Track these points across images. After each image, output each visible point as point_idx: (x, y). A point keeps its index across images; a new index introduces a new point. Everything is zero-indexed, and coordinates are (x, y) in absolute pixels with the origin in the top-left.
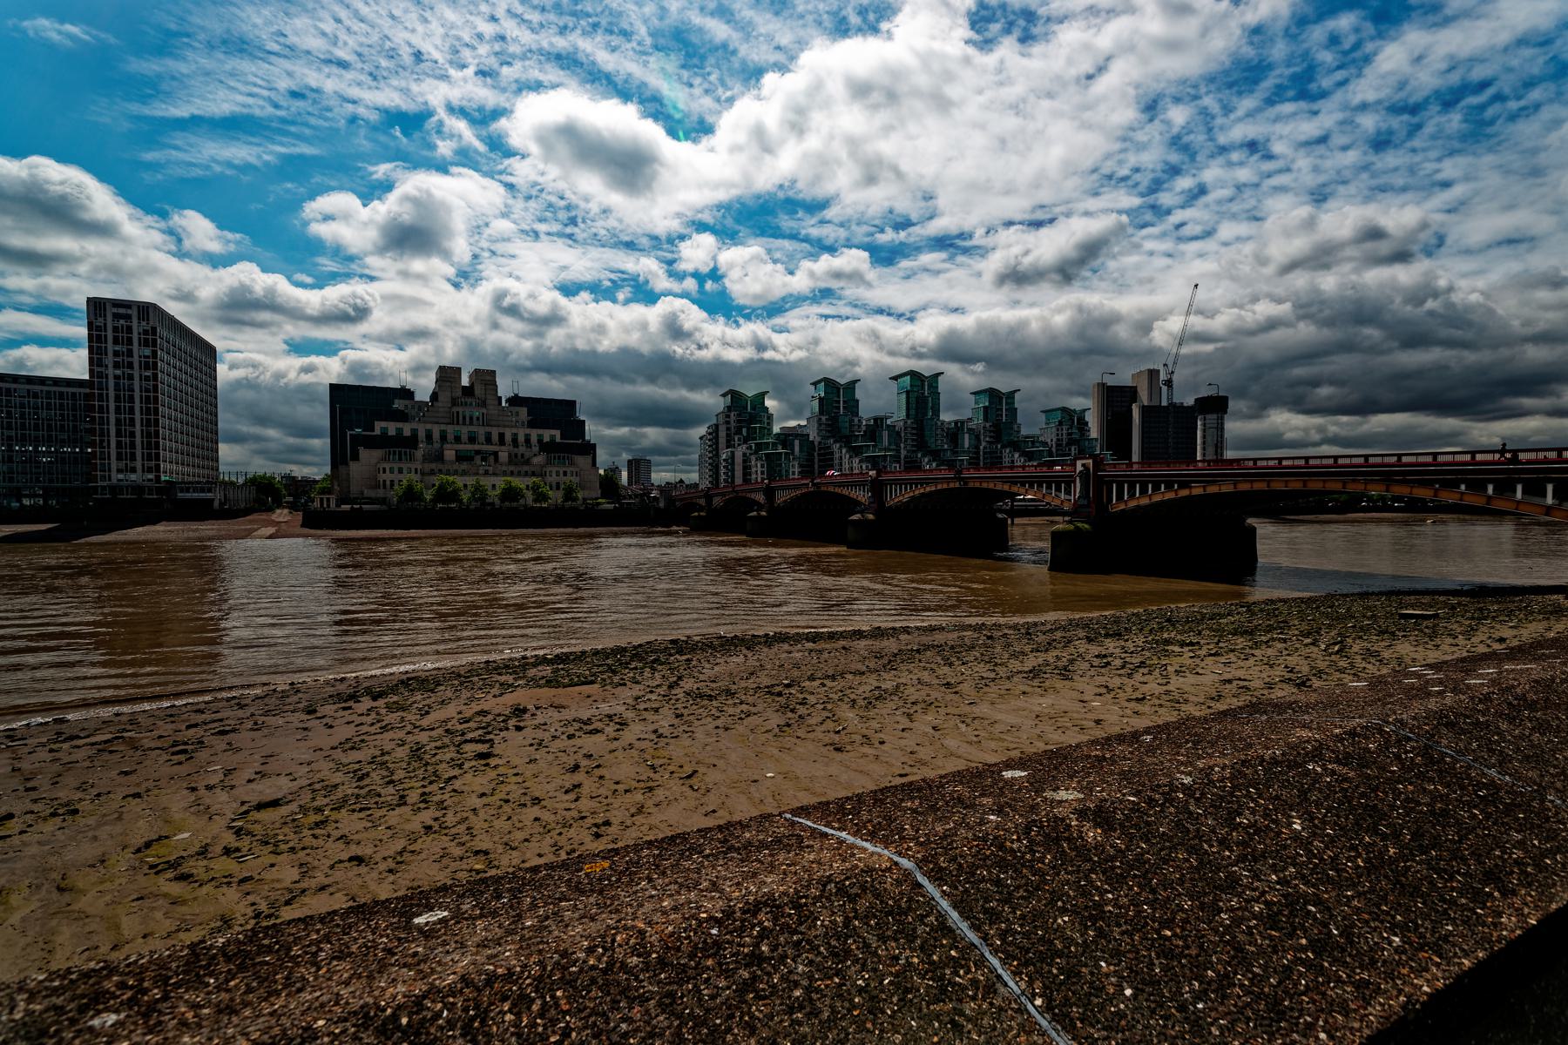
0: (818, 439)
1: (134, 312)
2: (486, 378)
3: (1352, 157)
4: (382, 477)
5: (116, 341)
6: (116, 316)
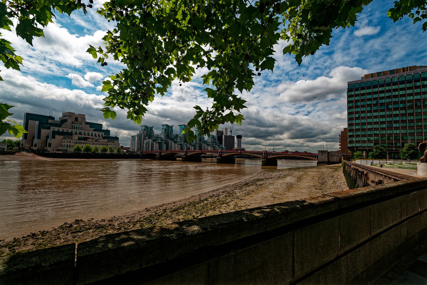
0: (164, 139)
2: (83, 117)
3: (260, 87)
4: (63, 144)
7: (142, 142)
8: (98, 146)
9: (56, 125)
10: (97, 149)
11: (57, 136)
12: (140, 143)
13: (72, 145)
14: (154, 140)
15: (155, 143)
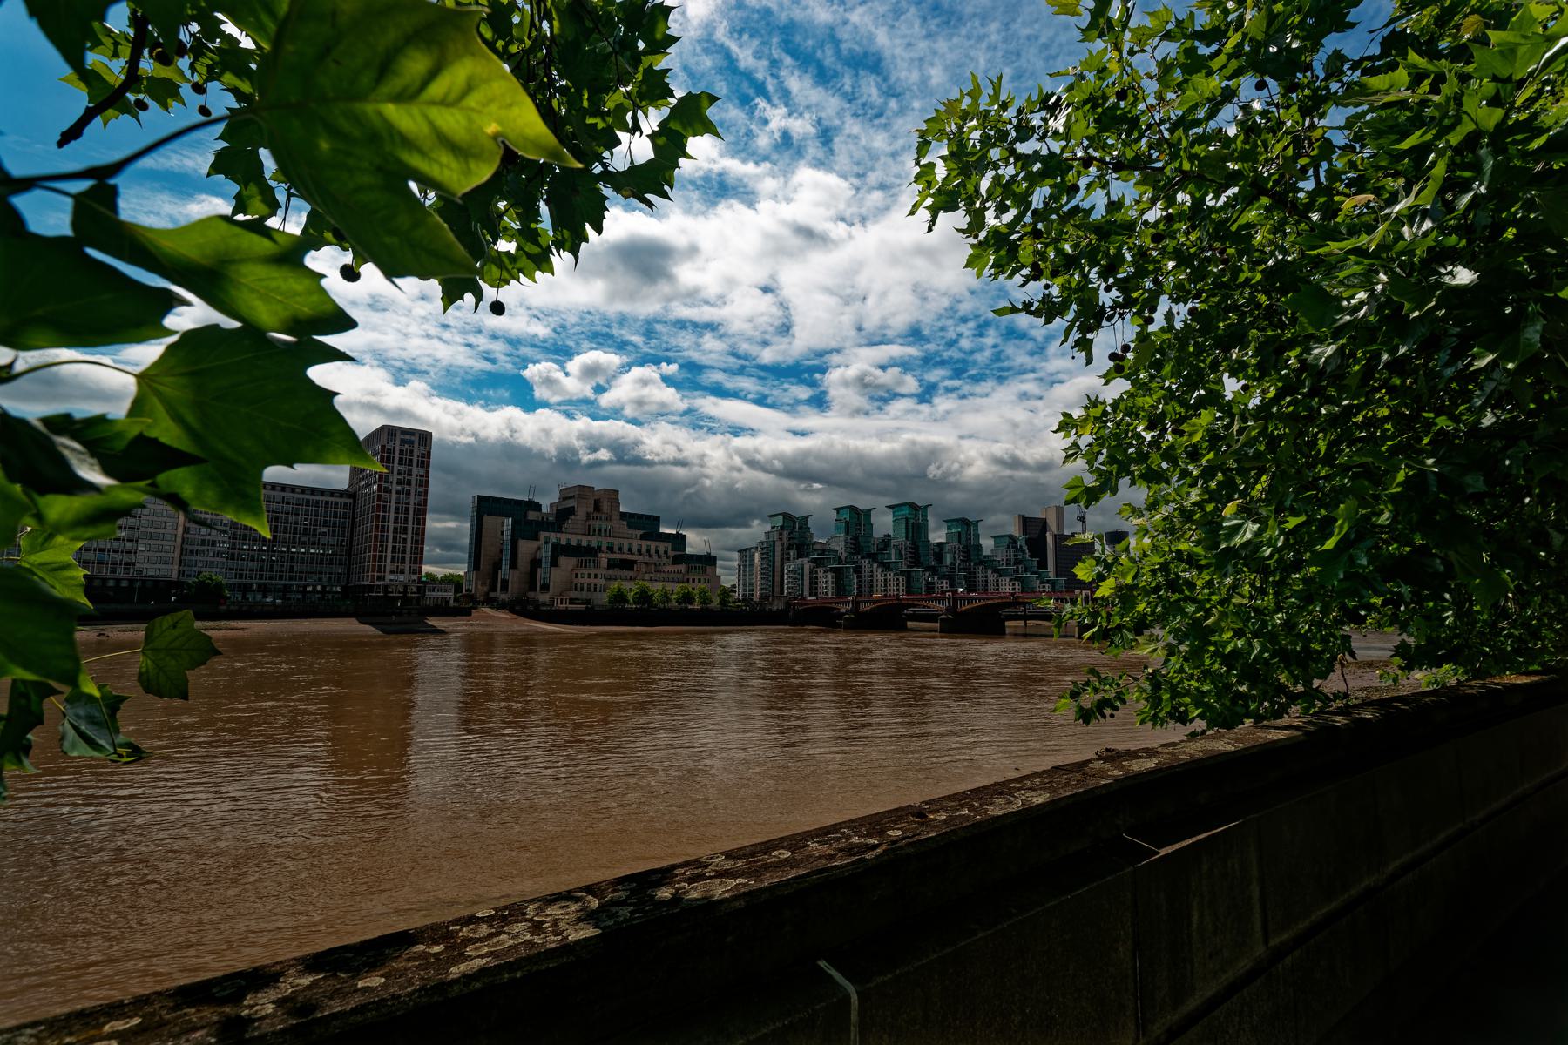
1: (416, 439)
2: (613, 496)
4: (579, 581)
5: (401, 462)
6: (403, 442)
7: (778, 569)
8: (669, 587)
9: (544, 525)
10: (666, 597)
11: (562, 560)
12: (771, 573)
13: (602, 586)
14: (818, 563)
15: (821, 571)
